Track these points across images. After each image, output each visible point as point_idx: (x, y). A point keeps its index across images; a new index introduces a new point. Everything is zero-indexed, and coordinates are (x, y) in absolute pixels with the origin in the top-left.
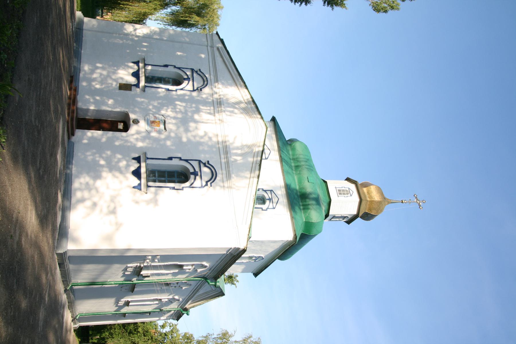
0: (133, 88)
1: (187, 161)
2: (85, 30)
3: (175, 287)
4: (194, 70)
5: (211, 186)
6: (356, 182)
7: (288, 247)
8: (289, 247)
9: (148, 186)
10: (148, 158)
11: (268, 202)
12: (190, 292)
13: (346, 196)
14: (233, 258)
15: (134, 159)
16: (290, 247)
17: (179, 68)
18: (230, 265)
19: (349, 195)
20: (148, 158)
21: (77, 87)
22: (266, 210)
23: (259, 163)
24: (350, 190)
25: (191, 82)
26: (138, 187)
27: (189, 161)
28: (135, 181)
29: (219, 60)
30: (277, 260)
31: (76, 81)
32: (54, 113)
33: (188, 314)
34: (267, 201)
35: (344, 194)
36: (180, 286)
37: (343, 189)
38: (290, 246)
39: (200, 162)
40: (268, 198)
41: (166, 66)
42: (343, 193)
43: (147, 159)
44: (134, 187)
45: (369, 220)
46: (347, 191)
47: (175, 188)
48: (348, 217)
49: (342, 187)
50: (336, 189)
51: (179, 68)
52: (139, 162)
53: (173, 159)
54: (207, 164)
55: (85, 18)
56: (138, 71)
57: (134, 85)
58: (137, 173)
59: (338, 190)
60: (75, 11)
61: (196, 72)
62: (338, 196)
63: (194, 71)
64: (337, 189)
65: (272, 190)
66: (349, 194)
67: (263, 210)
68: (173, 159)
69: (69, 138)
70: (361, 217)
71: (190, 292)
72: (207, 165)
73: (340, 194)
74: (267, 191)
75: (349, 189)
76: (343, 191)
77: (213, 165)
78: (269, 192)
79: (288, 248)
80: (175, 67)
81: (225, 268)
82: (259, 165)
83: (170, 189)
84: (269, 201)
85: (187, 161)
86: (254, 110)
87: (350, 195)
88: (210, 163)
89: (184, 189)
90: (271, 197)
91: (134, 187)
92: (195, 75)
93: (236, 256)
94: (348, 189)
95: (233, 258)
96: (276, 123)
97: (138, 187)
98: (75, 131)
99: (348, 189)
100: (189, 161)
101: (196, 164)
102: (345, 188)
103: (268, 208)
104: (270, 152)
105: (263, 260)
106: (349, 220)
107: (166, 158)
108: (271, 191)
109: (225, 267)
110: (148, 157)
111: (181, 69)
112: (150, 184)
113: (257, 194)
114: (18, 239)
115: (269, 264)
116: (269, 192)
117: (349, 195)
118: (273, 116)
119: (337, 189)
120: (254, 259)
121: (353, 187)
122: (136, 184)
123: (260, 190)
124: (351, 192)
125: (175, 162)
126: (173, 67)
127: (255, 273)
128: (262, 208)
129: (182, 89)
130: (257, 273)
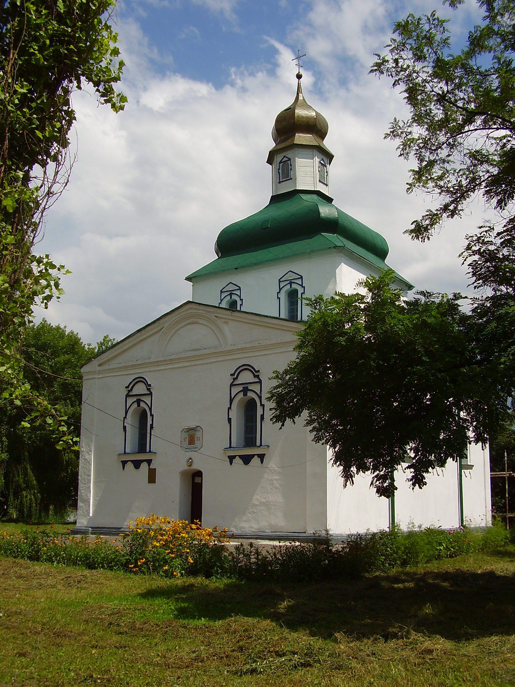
1: (231, 401)
2: (486, 524)
5: (259, 371)
9: (150, 451)
11: (294, 286)
17: (126, 412)
22: (304, 287)
25: (142, 398)
27: (232, 397)
28: (256, 461)
29: (114, 364)
32: (274, 547)
34: (292, 287)
37: (280, 171)
40: (289, 285)
41: (230, 420)
44: (262, 462)
49: (279, 173)
51: (126, 412)
52: (234, 457)
54: (235, 376)
56: (241, 457)
57: (149, 465)
58: (247, 459)
60: (76, 528)
62: (291, 179)
64: (281, 180)
65: (279, 280)
67: (242, 304)
72: (130, 389)
74: (281, 287)
75: (280, 163)
80: (230, 408)
84: (293, 285)
85: (231, 401)
90: (229, 293)
91: (262, 462)
92: (134, 392)
97: (262, 457)
99: (281, 164)
101: (235, 390)
102: (279, 169)
103: (302, 285)
104: (230, 284)
108: (280, 281)
112: (258, 443)
116: (223, 295)
122: (259, 460)
124: (285, 159)
125: (234, 415)
128: (302, 294)
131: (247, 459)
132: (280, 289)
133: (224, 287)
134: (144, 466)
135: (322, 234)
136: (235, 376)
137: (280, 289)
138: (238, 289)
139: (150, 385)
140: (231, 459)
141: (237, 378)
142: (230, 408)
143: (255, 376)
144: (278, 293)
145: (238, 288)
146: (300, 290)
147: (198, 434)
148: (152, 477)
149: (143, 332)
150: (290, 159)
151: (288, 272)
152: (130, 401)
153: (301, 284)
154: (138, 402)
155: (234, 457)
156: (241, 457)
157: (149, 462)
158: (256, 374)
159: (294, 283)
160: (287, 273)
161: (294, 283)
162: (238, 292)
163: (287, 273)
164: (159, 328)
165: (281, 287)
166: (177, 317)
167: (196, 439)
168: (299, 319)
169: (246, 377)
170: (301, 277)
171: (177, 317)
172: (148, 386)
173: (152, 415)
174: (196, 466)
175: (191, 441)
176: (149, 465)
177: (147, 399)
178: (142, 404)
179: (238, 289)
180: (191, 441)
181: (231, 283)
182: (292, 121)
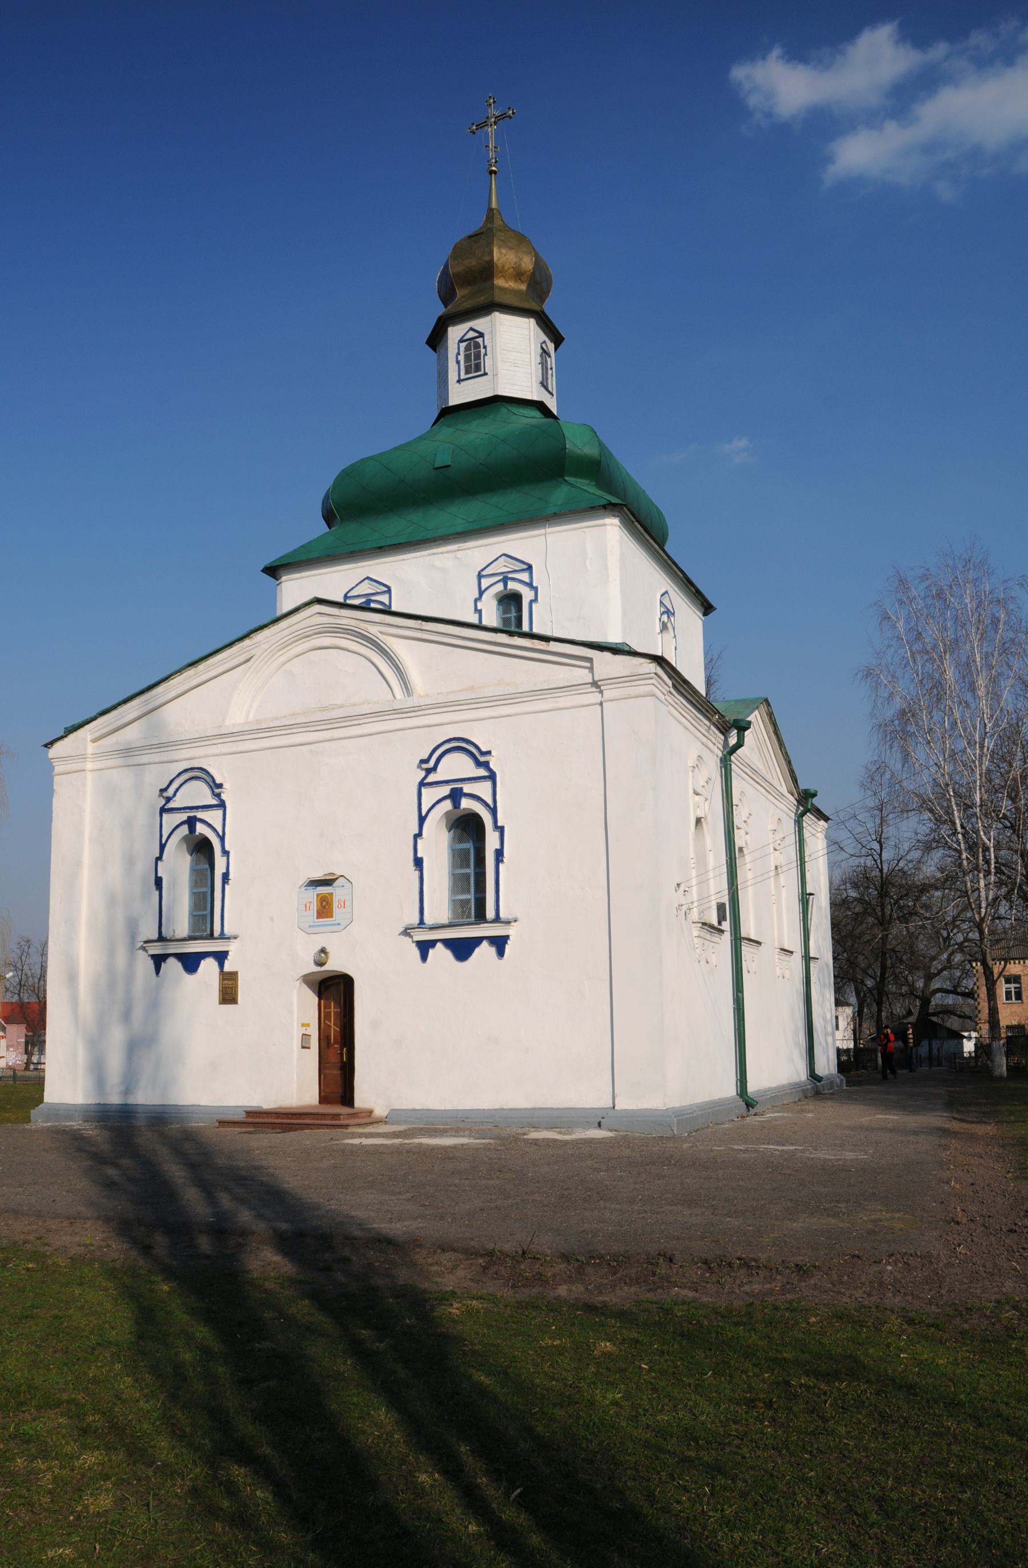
0: (228, 967)
1: (422, 820)
3: (747, 833)
4: (165, 805)
5: (489, 753)
6: (440, 319)
7: (637, 528)
8: (636, 523)
9: (497, 919)
10: (422, 922)
11: (512, 586)
12: (758, 791)
13: (483, 351)
14: (679, 687)
15: (424, 957)
16: (637, 521)
18: (697, 696)
19: (480, 340)
20: (422, 922)
21: (248, 1109)
22: (536, 589)
23: (420, 622)
24: (465, 338)
26: (500, 944)
27: (424, 813)
28: (485, 951)
30: (666, 548)
31: (163, 1113)
33: (814, 795)
35: (478, 356)
36: (745, 822)
38: (634, 520)
39: (422, 784)
42: (475, 360)
43: (424, 924)
45: (550, 276)
46: (467, 348)
47: (498, 847)
48: (544, 342)
50: (464, 380)
52: (432, 943)
53: (419, 855)
54: (428, 766)
55: (45, 1101)
56: (448, 943)
57: (221, 965)
58: (462, 949)
59: (467, 372)
61: (168, 800)
62: (485, 374)
63: (166, 807)
64: (463, 376)
66: (476, 340)
68: (419, 855)
69: (379, 1121)
70: (543, 301)
71: (758, 791)
73: (478, 368)
74: (483, 589)
75: (461, 341)
76: (467, 358)
77: (432, 748)
78: (483, 580)
79: (639, 526)
81: (702, 706)
82: (424, 623)
83: (502, 861)
86: (267, 637)
87: (481, 339)
88: (425, 757)
89: (499, 824)
93: (674, 682)
94: (463, 345)
95: (679, 687)
96: (279, 564)
97: (500, 944)
98: (358, 1108)
100: (424, 813)
101: (430, 796)
102: (458, 354)
103: (530, 585)
105: (671, 592)
106: (551, 341)
107: (417, 873)
108: (480, 576)
109: (700, 707)
110: (418, 922)
111: (163, 842)
113: (504, 626)
114: (202, 1332)
115: (681, 575)
116: (485, 583)
117: (480, 340)
118: (262, 571)
119: (463, 376)
120: (668, 617)
121: (455, 333)
122: (493, 950)
123: (479, 608)
124: (472, 334)
126: (159, 862)
127: (703, 610)
129: (222, 839)
130: (702, 604)
131: (462, 949)
132: (481, 593)
133: (354, 588)
134: (208, 966)
135: (566, 478)
136: (431, 764)
137: (481, 593)
138: (385, 592)
139: (220, 786)
140: (425, 948)
141: (434, 769)
142: (418, 835)
143: (479, 764)
144: (476, 601)
145: (386, 589)
146: (527, 595)
147: (338, 892)
148: (228, 995)
149: (201, 667)
150: (481, 335)
151: (500, 556)
152: (170, 820)
153: (527, 580)
154: (191, 822)
155: (432, 943)
156: (448, 943)
157: (221, 957)
158: (482, 759)
159: (513, 579)
160: (497, 559)
161: (513, 579)
162: (524, 577)
163: (497, 559)
164: (242, 658)
165: (483, 589)
166: (286, 632)
167: (335, 904)
168: (525, 628)
169: (456, 766)
170: (530, 568)
171: (286, 632)
172: (216, 787)
173: (226, 853)
174: (335, 965)
175: (325, 908)
176: (221, 965)
177: (213, 817)
178: (200, 828)
179: (385, 592)
180: (325, 908)
181: (368, 578)
182: (487, 258)
